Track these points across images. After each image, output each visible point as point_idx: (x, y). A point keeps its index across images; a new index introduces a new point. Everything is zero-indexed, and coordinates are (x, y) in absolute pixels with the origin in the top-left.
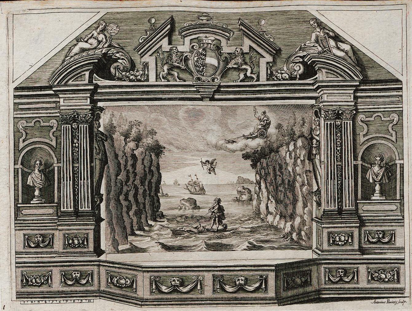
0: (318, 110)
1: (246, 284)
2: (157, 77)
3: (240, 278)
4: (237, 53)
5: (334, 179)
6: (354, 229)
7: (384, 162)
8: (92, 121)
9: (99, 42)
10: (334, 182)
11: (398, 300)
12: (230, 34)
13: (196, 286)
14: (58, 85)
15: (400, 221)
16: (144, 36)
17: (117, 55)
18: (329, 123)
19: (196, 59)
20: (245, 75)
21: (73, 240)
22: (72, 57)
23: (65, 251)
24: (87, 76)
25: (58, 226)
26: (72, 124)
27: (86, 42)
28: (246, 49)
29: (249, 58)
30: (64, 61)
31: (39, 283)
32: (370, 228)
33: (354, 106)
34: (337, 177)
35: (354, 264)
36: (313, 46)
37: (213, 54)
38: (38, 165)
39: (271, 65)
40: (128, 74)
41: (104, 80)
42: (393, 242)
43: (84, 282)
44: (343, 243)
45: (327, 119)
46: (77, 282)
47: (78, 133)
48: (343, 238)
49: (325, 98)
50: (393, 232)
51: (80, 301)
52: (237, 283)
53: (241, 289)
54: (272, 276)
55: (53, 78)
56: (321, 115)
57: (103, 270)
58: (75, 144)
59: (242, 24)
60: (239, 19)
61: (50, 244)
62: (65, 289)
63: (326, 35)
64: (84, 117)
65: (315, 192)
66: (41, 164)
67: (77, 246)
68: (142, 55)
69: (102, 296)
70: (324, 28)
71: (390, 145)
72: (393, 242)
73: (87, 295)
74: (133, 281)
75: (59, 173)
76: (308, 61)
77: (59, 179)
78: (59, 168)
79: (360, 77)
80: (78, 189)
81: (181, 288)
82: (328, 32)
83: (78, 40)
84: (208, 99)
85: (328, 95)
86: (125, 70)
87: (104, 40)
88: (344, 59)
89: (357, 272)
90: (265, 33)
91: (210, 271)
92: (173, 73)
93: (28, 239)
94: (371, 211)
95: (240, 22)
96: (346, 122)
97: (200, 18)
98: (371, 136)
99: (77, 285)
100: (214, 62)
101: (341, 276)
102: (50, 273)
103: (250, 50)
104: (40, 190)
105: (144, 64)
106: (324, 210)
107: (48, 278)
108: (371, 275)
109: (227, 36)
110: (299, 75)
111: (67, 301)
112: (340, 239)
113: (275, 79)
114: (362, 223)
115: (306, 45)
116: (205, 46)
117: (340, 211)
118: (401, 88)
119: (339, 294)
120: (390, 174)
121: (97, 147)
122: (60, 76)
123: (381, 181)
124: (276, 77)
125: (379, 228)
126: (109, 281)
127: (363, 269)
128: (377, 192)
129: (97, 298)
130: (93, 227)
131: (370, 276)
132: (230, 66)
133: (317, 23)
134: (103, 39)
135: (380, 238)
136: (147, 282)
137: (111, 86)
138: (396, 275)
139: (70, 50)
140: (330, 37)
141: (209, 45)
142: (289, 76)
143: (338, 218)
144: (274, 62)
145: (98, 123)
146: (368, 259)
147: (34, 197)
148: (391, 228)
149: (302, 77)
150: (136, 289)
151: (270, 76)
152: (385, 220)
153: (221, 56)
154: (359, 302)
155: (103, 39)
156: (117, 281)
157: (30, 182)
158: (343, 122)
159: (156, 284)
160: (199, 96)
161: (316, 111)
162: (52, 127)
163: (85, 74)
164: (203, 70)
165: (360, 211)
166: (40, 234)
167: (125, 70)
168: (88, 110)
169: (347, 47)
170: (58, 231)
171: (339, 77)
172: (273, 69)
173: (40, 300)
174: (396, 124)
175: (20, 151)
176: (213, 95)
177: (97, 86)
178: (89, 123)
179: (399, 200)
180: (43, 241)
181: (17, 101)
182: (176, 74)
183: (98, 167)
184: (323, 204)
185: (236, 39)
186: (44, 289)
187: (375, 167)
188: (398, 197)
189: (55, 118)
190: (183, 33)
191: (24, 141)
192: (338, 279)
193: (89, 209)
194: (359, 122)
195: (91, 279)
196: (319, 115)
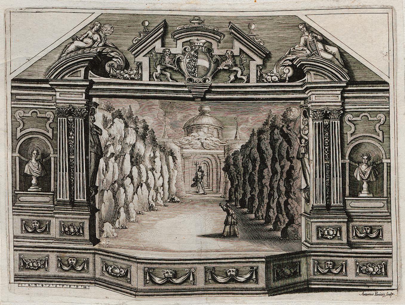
0: (306, 110)
1: (237, 275)
2: (151, 76)
3: (231, 270)
4: (227, 55)
5: (323, 177)
6: (342, 224)
7: (371, 161)
8: (87, 116)
9: (94, 42)
10: (322, 180)
11: (385, 292)
12: (220, 37)
13: (189, 278)
14: (55, 79)
15: (387, 217)
16: (137, 38)
17: (112, 54)
18: (317, 122)
19: (188, 60)
20: (236, 76)
21: (69, 228)
22: (68, 54)
23: (61, 237)
24: (83, 72)
25: (54, 214)
26: (68, 117)
27: (82, 41)
28: (236, 52)
29: (241, 61)
30: (60, 58)
31: (36, 267)
32: (357, 223)
33: (342, 106)
34: (326, 175)
35: (343, 257)
36: (302, 50)
37: (204, 56)
38: (35, 155)
39: (261, 67)
40: (122, 72)
41: (98, 76)
42: (380, 237)
43: (79, 268)
44: (332, 237)
45: (316, 119)
46: (73, 268)
47: (74, 126)
48: (331, 233)
49: (313, 98)
50: (381, 228)
51: (76, 287)
52: (229, 274)
53: (233, 280)
54: (262, 268)
55: (50, 72)
56: (309, 115)
57: (98, 258)
58: (71, 136)
59: (232, 28)
60: (230, 23)
61: (47, 230)
62: (63, 274)
63: (314, 39)
64: (80, 112)
65: (304, 189)
66: (38, 154)
67: (73, 234)
68: (136, 55)
69: (98, 284)
70: (312, 32)
71: (377, 145)
72: (380, 237)
73: (82, 281)
74: (128, 271)
75: (55, 164)
76: (298, 64)
77: (55, 169)
78: (56, 159)
79: (347, 78)
80: (74, 180)
81: (174, 280)
82: (316, 35)
83: (74, 38)
84: (200, 99)
85: (316, 95)
86: (120, 68)
87: (99, 40)
88: (330, 61)
89: (346, 264)
90: (255, 37)
91: (203, 263)
92: (165, 73)
93: (25, 225)
94: (357, 207)
95: (230, 25)
96: (333, 121)
97: (192, 22)
98: (358, 136)
99: (73, 272)
100: (206, 64)
101: (329, 268)
102: (47, 257)
103: (240, 54)
104: (37, 178)
105: (138, 64)
106: (313, 205)
107: (45, 262)
108: (359, 268)
109: (217, 39)
110: (288, 78)
111: (63, 285)
112: (328, 232)
113: (265, 81)
114: (350, 218)
115: (296, 48)
116: (197, 48)
117: (328, 207)
118: (388, 90)
119: (328, 285)
120: (377, 173)
121: (92, 140)
122: (57, 70)
123: (369, 179)
124: (266, 79)
125: (366, 224)
126: (104, 269)
127: (351, 262)
128: (365, 189)
129: (93, 285)
130: (88, 217)
131: (358, 269)
132: (221, 68)
133: (306, 28)
134: (98, 39)
135: (368, 233)
136: (141, 274)
137: (106, 82)
138: (383, 268)
139: (66, 47)
140: (318, 41)
141: (201, 47)
142: (279, 79)
143: (327, 213)
144: (264, 65)
145: (93, 117)
146: (356, 253)
147: (31, 185)
148: (378, 224)
149: (291, 79)
150: (130, 279)
151: (260, 78)
152: (372, 216)
153: (212, 58)
154: (347, 293)
155: (98, 39)
156: (112, 270)
157: (27, 170)
158: (331, 121)
159: (149, 274)
160: (191, 96)
161: (304, 111)
162: (48, 119)
163: (81, 70)
164: (195, 72)
165: (348, 208)
166: (37, 221)
167: (120, 68)
168: (84, 105)
169: (334, 50)
170: (55, 218)
171: (326, 79)
172: (262, 71)
173: (37, 283)
174: (383, 124)
175: (19, 140)
176: (205, 95)
177: (92, 83)
178: (85, 117)
179: (386, 197)
180: (40, 228)
181: (14, 91)
182: (168, 75)
183: (93, 160)
184: (311, 199)
185: (226, 42)
186: (41, 272)
187: (362, 166)
188: (385, 195)
189: (51, 110)
190: (176, 36)
191: (21, 131)
192: (327, 271)
193: (84, 200)
194: (346, 122)
195: (87, 266)
196: (308, 115)
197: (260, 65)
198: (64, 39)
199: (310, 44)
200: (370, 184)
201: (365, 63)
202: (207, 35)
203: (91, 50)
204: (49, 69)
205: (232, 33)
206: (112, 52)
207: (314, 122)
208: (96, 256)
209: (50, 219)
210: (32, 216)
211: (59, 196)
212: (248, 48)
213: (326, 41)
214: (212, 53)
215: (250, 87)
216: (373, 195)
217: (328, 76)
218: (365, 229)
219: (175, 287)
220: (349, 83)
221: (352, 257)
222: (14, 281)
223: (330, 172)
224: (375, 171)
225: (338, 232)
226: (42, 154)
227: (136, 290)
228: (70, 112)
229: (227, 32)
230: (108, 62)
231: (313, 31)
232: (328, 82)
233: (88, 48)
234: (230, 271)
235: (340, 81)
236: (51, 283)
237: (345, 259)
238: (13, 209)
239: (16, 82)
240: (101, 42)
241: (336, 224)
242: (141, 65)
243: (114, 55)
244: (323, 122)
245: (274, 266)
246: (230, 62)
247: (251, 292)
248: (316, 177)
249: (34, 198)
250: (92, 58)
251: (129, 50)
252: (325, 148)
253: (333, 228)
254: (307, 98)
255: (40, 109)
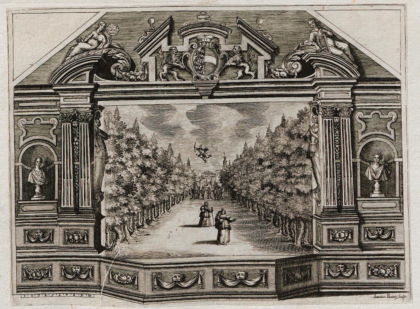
1: (246, 278)
2: (157, 77)
3: (240, 273)
4: (235, 51)
5: (334, 177)
7: (383, 160)
8: (92, 120)
9: (99, 43)
12: (228, 32)
13: (197, 281)
14: (60, 84)
16: (143, 37)
17: (118, 55)
21: (73, 236)
22: (72, 57)
25: (58, 222)
26: (72, 122)
27: (87, 42)
28: (244, 48)
29: (247, 56)
32: (370, 225)
34: (337, 175)
35: (355, 259)
36: (312, 45)
37: (212, 53)
38: (39, 163)
39: (269, 63)
40: (128, 74)
44: (343, 240)
45: (325, 117)
47: (79, 131)
48: (343, 235)
49: (323, 95)
50: (393, 229)
51: (80, 295)
52: (238, 277)
53: (241, 283)
54: (272, 271)
56: (319, 112)
58: (76, 142)
59: (240, 23)
60: (237, 18)
61: (50, 240)
63: (324, 35)
64: (84, 116)
66: (41, 162)
67: (77, 242)
71: (388, 143)
73: (86, 290)
75: (60, 171)
80: (79, 187)
81: (182, 283)
82: (326, 31)
83: (78, 40)
85: (325, 92)
86: (126, 69)
87: (104, 41)
88: (341, 57)
89: (357, 266)
92: (173, 72)
93: (28, 234)
95: (238, 20)
96: (344, 119)
98: (370, 133)
99: (77, 280)
100: (213, 60)
101: (340, 271)
102: (50, 267)
104: (41, 186)
105: (144, 64)
106: (324, 207)
107: (48, 272)
108: (371, 271)
111: (67, 294)
112: (340, 235)
113: (273, 76)
114: (362, 220)
115: (305, 44)
116: (204, 45)
117: (340, 208)
120: (389, 172)
122: (61, 75)
123: (381, 179)
124: (274, 75)
125: (377, 225)
126: (111, 277)
127: (363, 265)
128: (376, 189)
131: (370, 271)
132: (228, 64)
133: (316, 24)
136: (149, 279)
138: (395, 270)
140: (328, 36)
141: (208, 43)
144: (272, 61)
145: (98, 121)
147: (34, 193)
148: (390, 225)
149: (300, 75)
150: (138, 285)
151: (268, 74)
153: (219, 54)
156: (118, 278)
158: (341, 119)
160: (198, 95)
162: (52, 125)
164: (202, 69)
165: (360, 209)
166: (40, 230)
169: (344, 46)
170: (58, 227)
171: (336, 75)
174: (395, 122)
175: (21, 148)
176: (213, 93)
177: (97, 86)
178: (90, 122)
179: (398, 198)
185: (233, 37)
186: (45, 282)
188: (398, 195)
189: (56, 116)
191: (24, 139)
193: (89, 206)
194: (357, 120)
197: (269, 60)
198: (67, 42)
199: (319, 40)
200: (382, 184)
201: (374, 58)
202: (214, 30)
203: (96, 52)
204: (53, 74)
205: (240, 27)
206: (118, 53)
207: (324, 120)
208: (102, 263)
209: (54, 227)
210: (34, 225)
211: (63, 203)
212: (255, 43)
213: (335, 36)
214: (219, 49)
215: (258, 83)
216: (385, 195)
217: (338, 72)
218: (377, 230)
219: (184, 291)
220: (359, 80)
221: (363, 259)
222: (17, 293)
223: (341, 172)
224: (387, 171)
225: (350, 235)
226: (46, 162)
227: (144, 296)
228: (74, 117)
229: (234, 26)
230: (113, 64)
231: (323, 27)
232: (336, 79)
233: (92, 50)
234: (239, 274)
235: (350, 77)
236: (55, 293)
237: (357, 261)
238: (16, 220)
239: (19, 89)
240: (106, 43)
241: (348, 226)
242: (147, 65)
243: (119, 57)
244: (333, 120)
245: (284, 270)
246: (238, 58)
247: (260, 296)
248: (327, 177)
249: (36, 208)
250: (97, 61)
251: (134, 50)
252: (335, 147)
253: (345, 231)
254: (317, 95)
255: (43, 116)
